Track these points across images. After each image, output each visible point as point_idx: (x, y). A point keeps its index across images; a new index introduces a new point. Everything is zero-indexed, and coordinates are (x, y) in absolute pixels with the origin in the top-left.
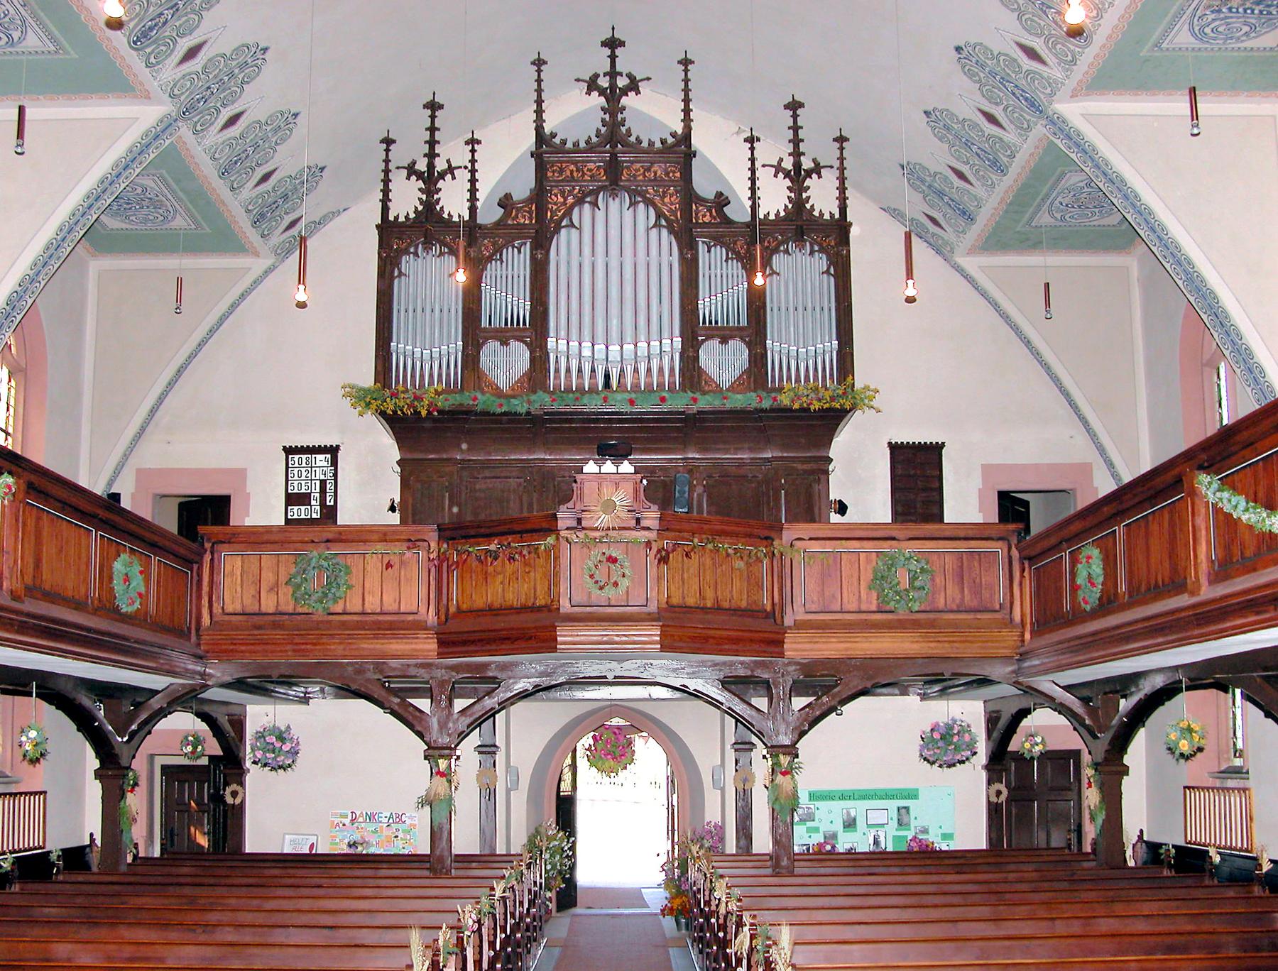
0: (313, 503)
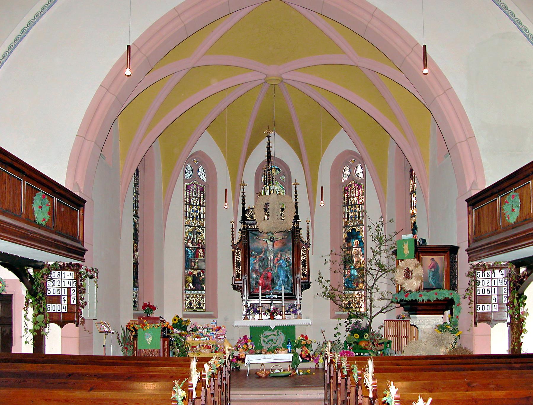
0: (493, 302)
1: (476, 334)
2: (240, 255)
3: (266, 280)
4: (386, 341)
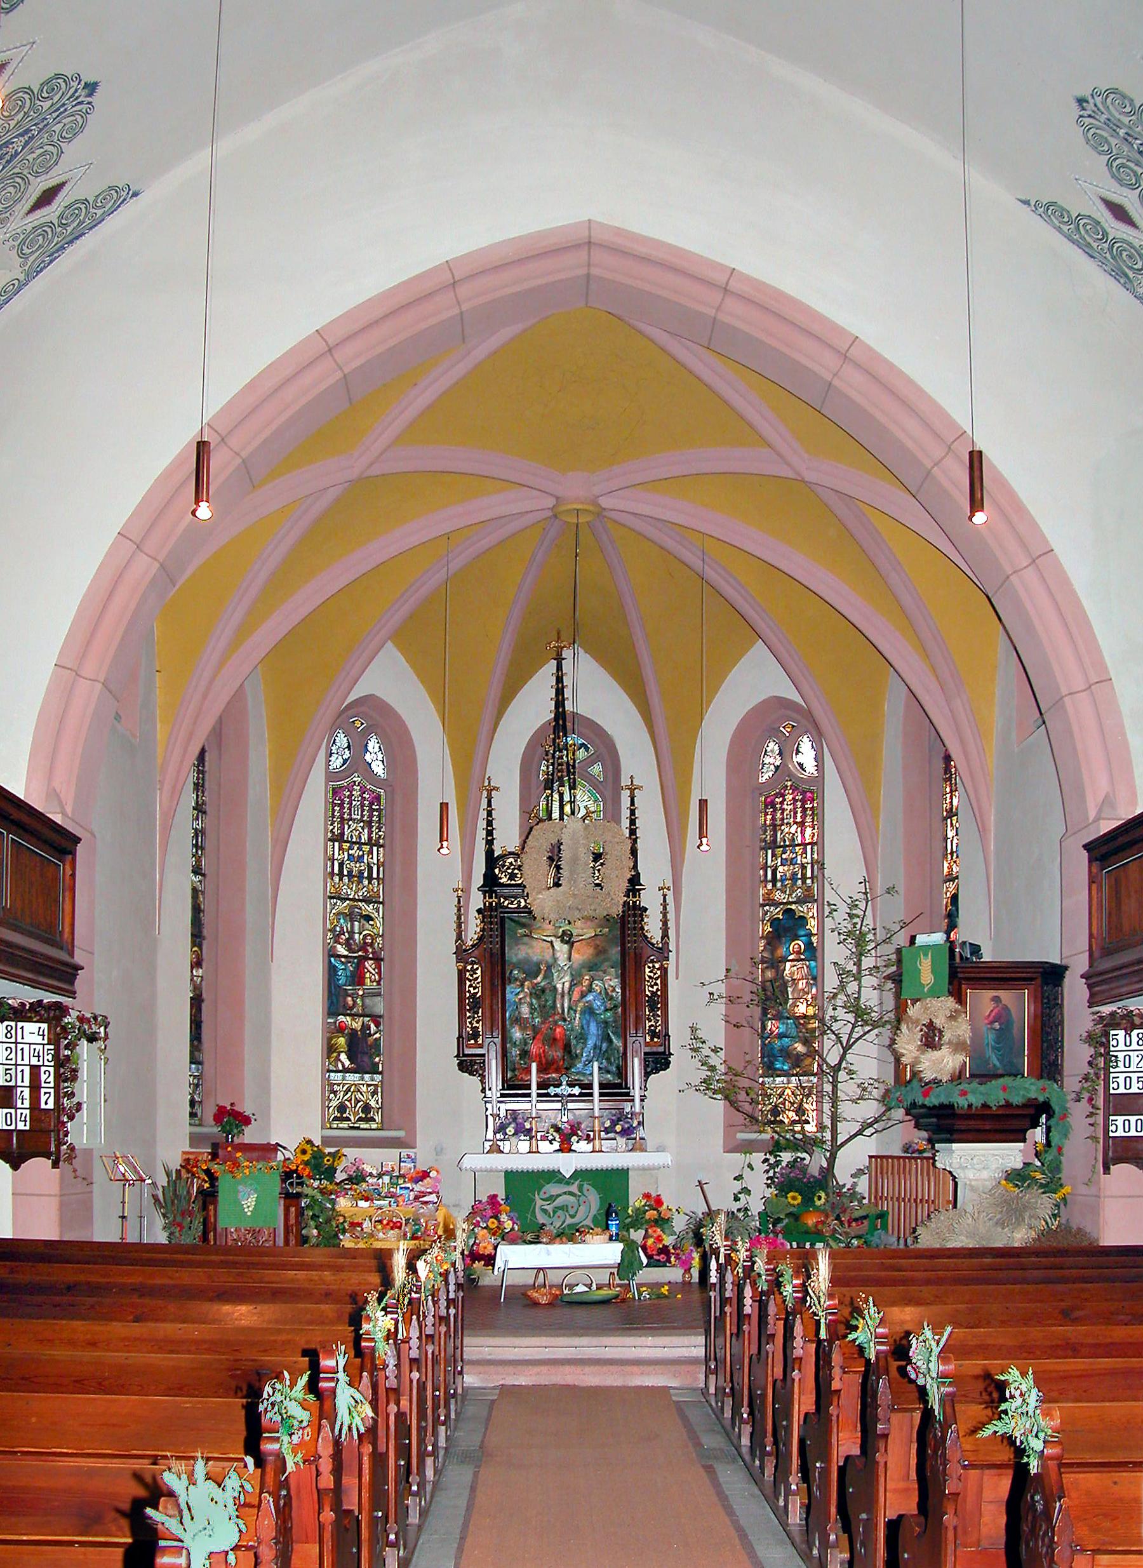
1: (1108, 1193)
2: (479, 980)
3: (550, 1046)
4: (873, 1211)
